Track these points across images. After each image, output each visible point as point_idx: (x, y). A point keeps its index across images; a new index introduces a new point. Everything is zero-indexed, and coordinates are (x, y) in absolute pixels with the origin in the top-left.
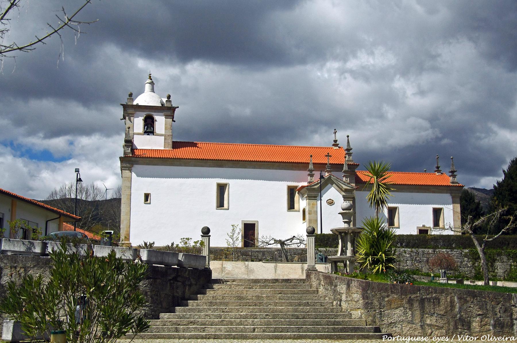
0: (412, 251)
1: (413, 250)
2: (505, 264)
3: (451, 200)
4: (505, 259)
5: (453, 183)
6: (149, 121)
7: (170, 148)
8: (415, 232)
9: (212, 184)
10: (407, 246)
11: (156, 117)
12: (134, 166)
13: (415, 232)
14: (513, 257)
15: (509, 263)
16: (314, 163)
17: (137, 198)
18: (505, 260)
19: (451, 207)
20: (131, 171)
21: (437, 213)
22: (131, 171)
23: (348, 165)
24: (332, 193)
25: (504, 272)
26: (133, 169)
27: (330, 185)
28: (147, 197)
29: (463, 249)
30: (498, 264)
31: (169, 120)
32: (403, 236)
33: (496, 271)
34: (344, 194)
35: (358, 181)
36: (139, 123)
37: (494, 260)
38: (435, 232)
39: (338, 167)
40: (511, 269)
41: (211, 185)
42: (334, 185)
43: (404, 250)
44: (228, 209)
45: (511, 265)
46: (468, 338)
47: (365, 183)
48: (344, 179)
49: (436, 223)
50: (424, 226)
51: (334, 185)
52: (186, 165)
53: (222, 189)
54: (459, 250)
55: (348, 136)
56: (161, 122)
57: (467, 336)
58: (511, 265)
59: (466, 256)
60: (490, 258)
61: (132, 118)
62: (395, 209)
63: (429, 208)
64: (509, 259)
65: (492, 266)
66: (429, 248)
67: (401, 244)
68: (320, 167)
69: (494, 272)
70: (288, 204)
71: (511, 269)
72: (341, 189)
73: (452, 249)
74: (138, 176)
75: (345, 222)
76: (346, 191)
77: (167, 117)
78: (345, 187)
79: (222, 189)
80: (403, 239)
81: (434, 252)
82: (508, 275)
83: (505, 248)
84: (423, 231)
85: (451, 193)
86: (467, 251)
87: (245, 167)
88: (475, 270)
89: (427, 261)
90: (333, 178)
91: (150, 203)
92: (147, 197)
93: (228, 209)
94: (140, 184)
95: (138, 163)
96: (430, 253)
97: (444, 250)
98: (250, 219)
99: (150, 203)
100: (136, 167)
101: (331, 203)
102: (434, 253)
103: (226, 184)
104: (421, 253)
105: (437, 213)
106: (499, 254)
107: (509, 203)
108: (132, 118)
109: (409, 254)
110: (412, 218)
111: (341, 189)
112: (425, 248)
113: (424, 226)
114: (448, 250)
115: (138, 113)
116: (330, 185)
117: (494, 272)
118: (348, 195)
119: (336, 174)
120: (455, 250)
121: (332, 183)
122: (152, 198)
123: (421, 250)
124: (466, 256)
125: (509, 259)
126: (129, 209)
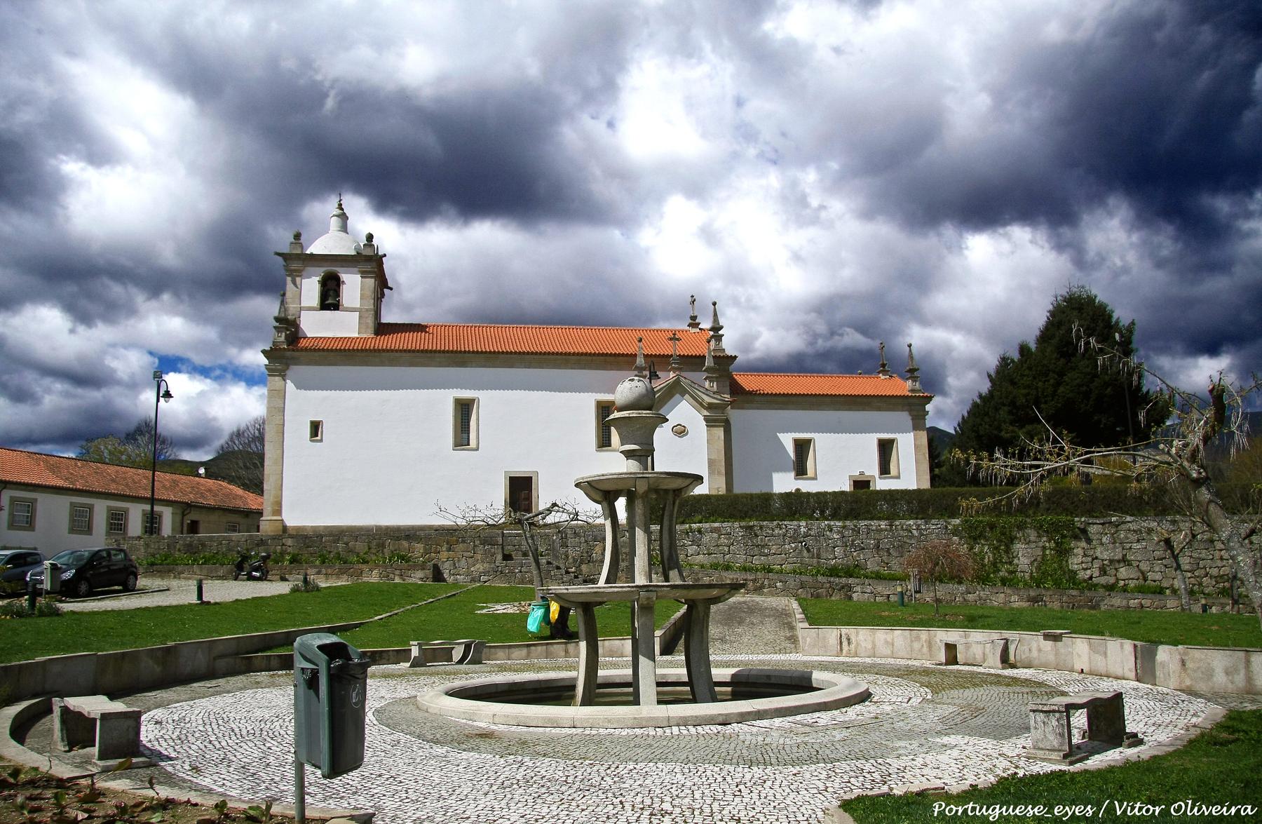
0: (844, 527)
1: (848, 523)
2: (1033, 545)
3: (910, 423)
4: (1032, 534)
5: (912, 391)
6: (331, 284)
7: (369, 334)
8: (847, 487)
9: (443, 401)
10: (834, 516)
11: (344, 277)
12: (293, 367)
13: (847, 487)
14: (1047, 532)
15: (1041, 544)
16: (646, 356)
17: (296, 430)
18: (1032, 538)
19: (911, 435)
20: (284, 378)
21: (886, 448)
22: (284, 378)
23: (714, 357)
24: (683, 412)
25: (1032, 563)
26: (289, 373)
27: (678, 396)
28: (316, 428)
29: (949, 517)
30: (1019, 547)
31: (368, 280)
32: (825, 493)
33: (1016, 561)
34: (706, 413)
35: (736, 389)
36: (310, 288)
37: (1012, 540)
38: (881, 484)
39: (694, 362)
40: (1044, 555)
41: (443, 401)
42: (687, 396)
43: (829, 526)
44: (477, 449)
45: (1044, 548)
46: (1140, 809)
47: (750, 393)
48: (707, 384)
49: (885, 470)
50: (862, 473)
51: (687, 396)
52: (392, 363)
53: (464, 410)
54: (942, 521)
55: (714, 304)
56: (353, 286)
57: (1138, 805)
58: (1044, 548)
59: (955, 532)
60: (1004, 534)
61: (298, 279)
62: (808, 442)
63: (870, 442)
64: (1039, 536)
65: (1008, 551)
66: (880, 519)
67: (822, 512)
68: (655, 364)
69: (1011, 563)
70: (598, 436)
71: (1044, 555)
72: (701, 404)
73: (927, 518)
74: (299, 386)
75: (629, 455)
76: (710, 407)
77: (364, 274)
78: (708, 400)
79: (464, 410)
80: (826, 502)
81: (891, 525)
82: (1038, 568)
83: (1031, 512)
84: (861, 484)
85: (910, 411)
86: (958, 521)
87: (511, 365)
88: (975, 561)
89: (877, 547)
90: (684, 382)
91: (321, 441)
92: (316, 428)
93: (477, 449)
94: (303, 403)
95: (297, 362)
96: (882, 530)
97: (911, 522)
98: (521, 469)
99: (321, 441)
100: (295, 370)
101: (681, 431)
102: (891, 530)
103: (473, 400)
104: (864, 529)
105: (886, 448)
106: (1021, 527)
107: (1011, 428)
108: (298, 279)
109: (839, 532)
110: (841, 458)
111: (700, 404)
112: (872, 519)
113: (862, 473)
114: (919, 522)
115: (310, 269)
116: (678, 396)
117: (1011, 563)
118: (716, 418)
119: (699, 376)
120: (933, 521)
121: (683, 392)
122: (326, 430)
123: (863, 523)
124: (955, 532)
125: (1039, 536)
126: (279, 452)
